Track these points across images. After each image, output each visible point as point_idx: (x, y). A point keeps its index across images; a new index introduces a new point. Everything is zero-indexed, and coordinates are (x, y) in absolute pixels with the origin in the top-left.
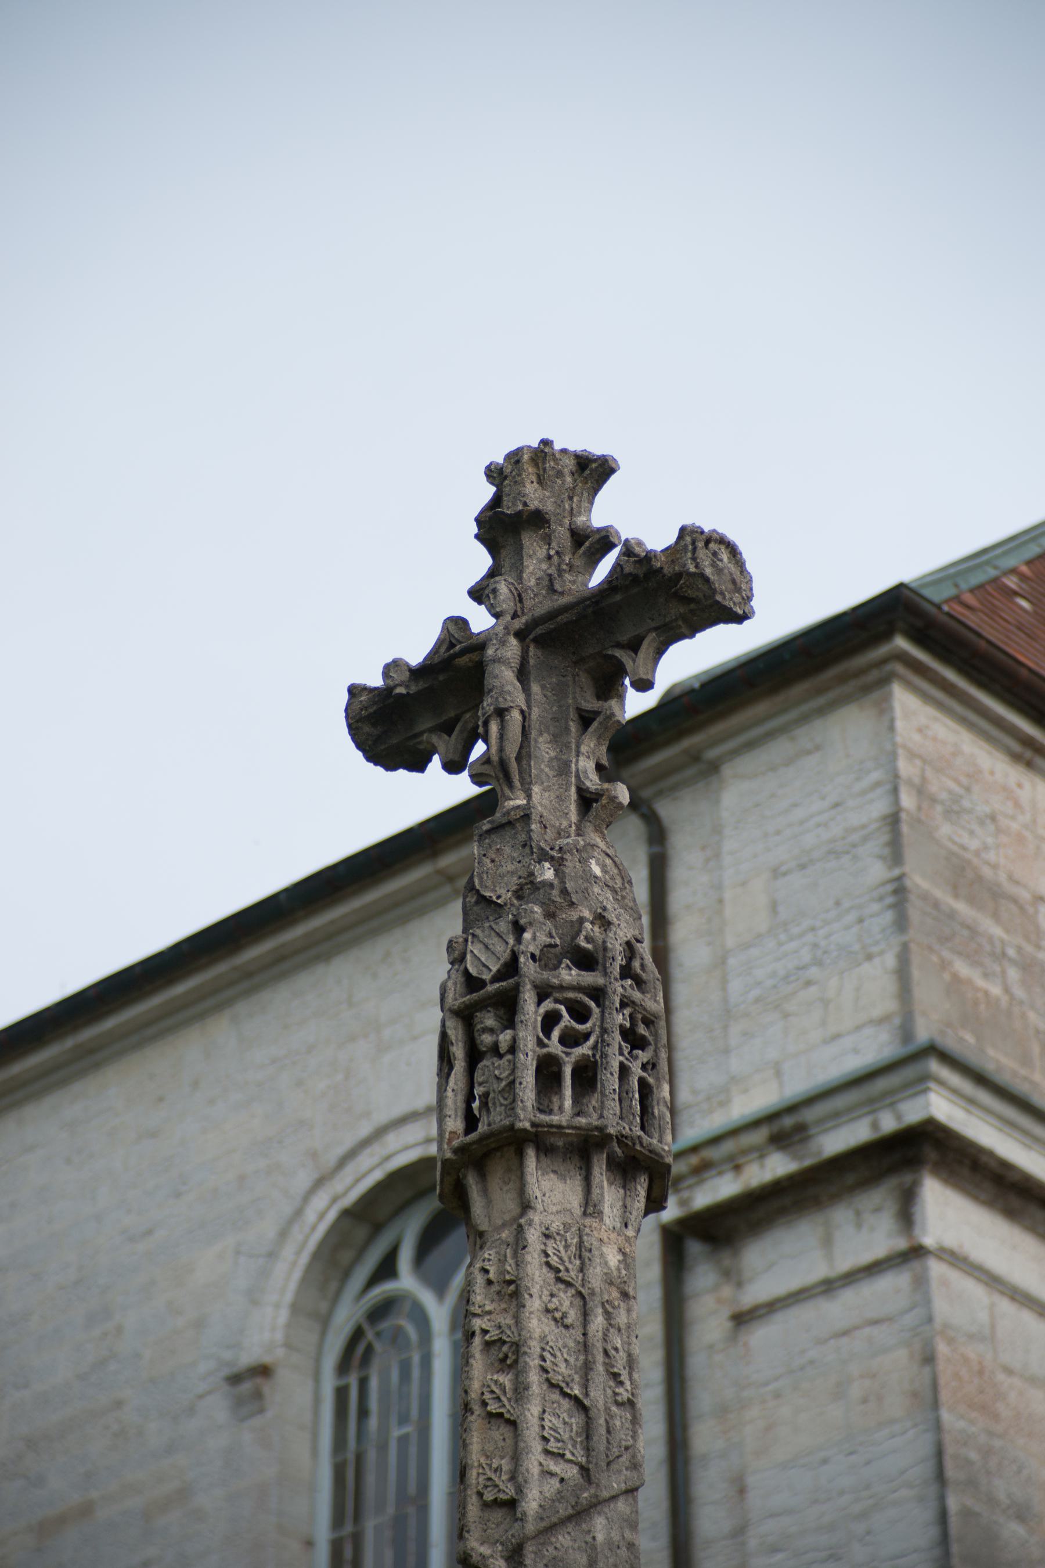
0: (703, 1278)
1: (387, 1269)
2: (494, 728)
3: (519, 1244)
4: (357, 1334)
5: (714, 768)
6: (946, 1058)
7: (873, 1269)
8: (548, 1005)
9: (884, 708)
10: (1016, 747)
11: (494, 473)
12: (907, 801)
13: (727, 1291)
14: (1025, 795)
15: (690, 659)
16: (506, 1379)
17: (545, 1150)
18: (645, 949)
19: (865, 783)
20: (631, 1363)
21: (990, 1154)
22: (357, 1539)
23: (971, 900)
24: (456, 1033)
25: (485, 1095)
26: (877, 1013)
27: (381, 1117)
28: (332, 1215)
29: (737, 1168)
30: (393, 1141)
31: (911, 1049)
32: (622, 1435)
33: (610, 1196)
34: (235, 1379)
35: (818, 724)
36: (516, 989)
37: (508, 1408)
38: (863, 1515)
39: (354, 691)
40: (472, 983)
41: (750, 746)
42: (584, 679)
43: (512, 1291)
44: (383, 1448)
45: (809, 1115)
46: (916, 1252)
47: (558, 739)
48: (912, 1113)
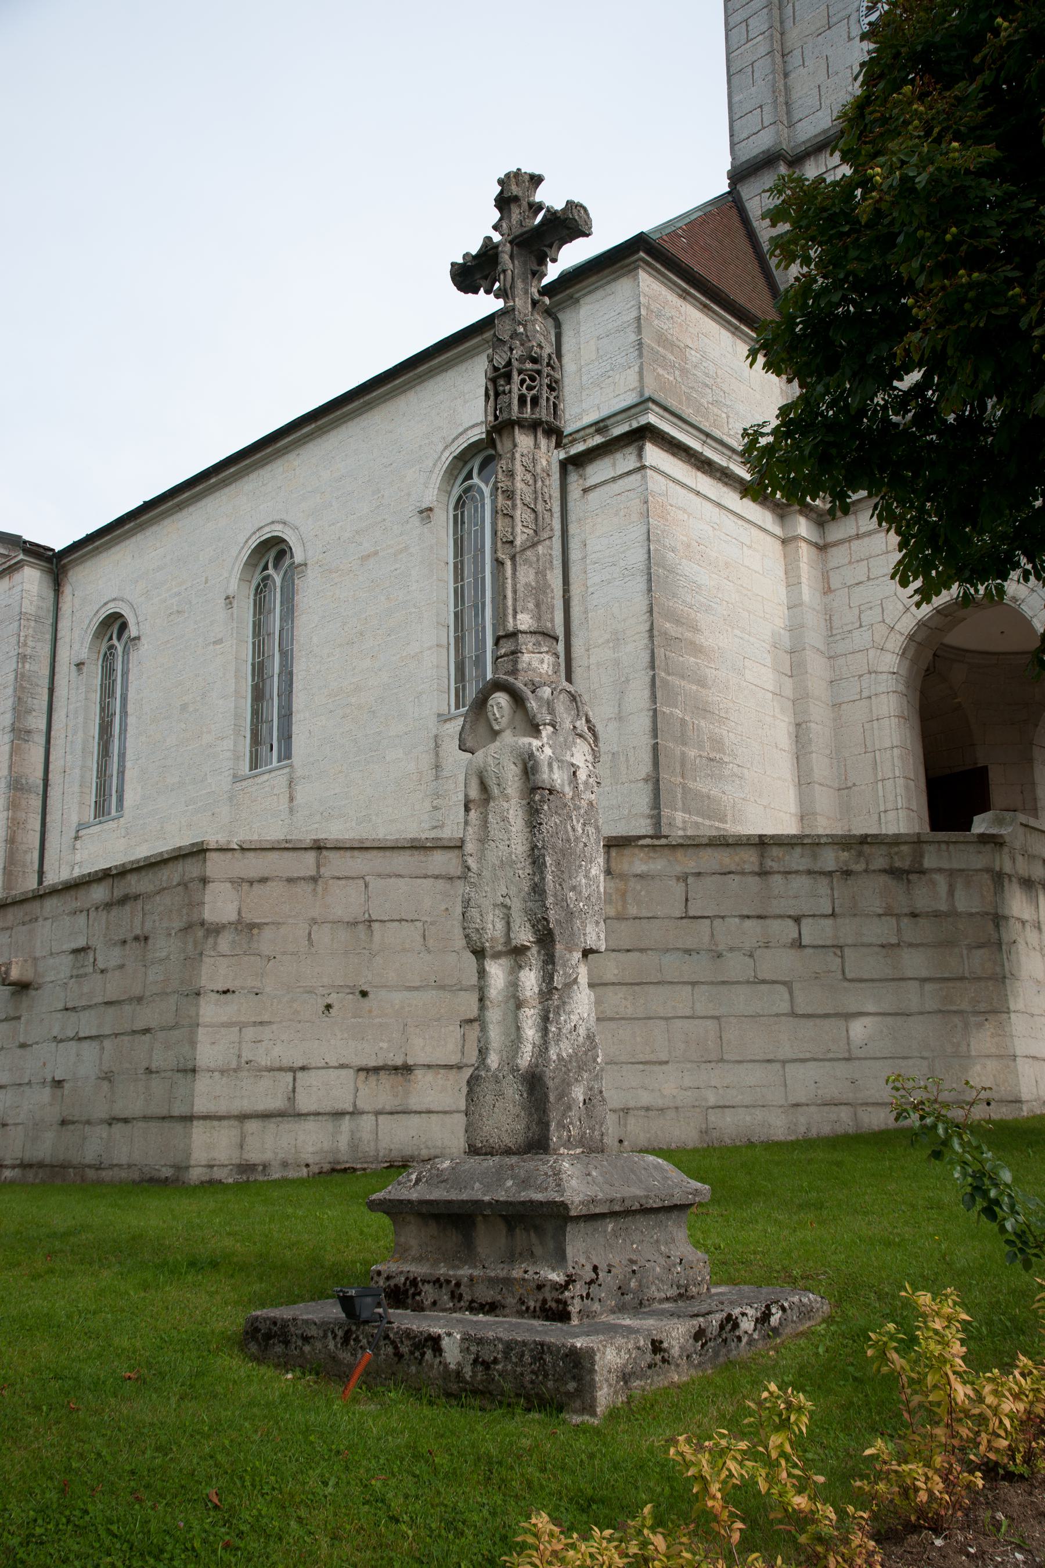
0: (573, 477)
1: (469, 476)
2: (502, 277)
3: (513, 458)
4: (460, 498)
5: (577, 301)
6: (654, 402)
7: (629, 473)
8: (522, 376)
9: (636, 278)
10: (681, 293)
11: (501, 182)
12: (643, 312)
13: (581, 481)
14: (683, 310)
15: (572, 255)
16: (509, 503)
17: (521, 426)
18: (554, 356)
19: (629, 306)
20: (550, 497)
21: (668, 434)
22: (462, 562)
23: (664, 347)
24: (490, 387)
25: (501, 409)
26: (631, 387)
27: (466, 425)
28: (450, 458)
29: (585, 441)
30: (470, 433)
31: (643, 399)
32: (548, 520)
33: (543, 442)
34: (421, 512)
35: (613, 284)
36: (511, 371)
37: (510, 512)
38: (624, 552)
39: (453, 264)
40: (496, 369)
41: (590, 292)
42: (533, 258)
43: (511, 474)
44: (469, 534)
45: (609, 422)
46: (643, 467)
47: (524, 281)
48: (643, 421)
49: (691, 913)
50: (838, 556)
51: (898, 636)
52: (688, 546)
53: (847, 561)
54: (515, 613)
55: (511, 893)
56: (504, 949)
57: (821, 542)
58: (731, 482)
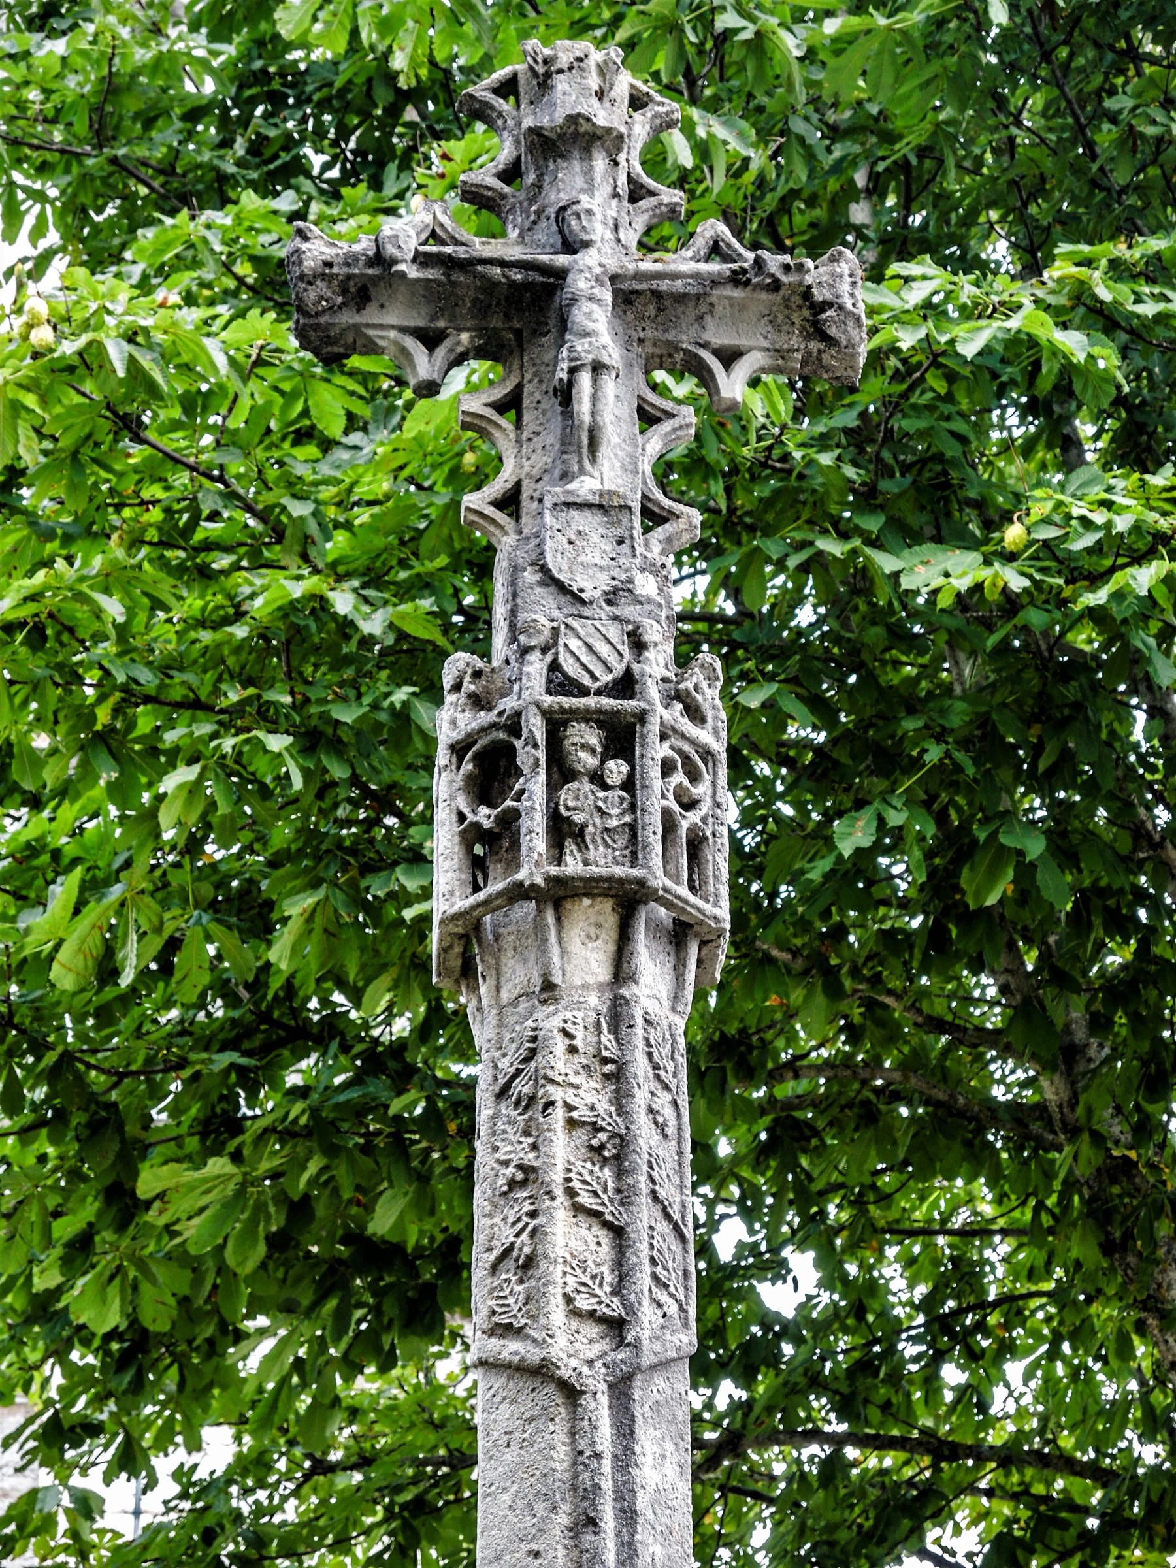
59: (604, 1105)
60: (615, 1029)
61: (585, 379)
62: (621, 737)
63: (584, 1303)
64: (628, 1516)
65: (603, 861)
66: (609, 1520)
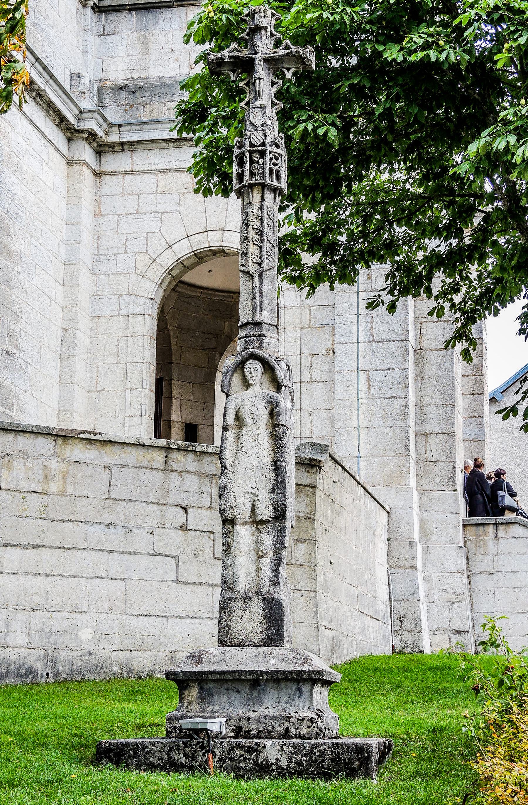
49: (112, 496)
50: (110, 184)
51: (159, 268)
52: (10, 157)
53: (119, 191)
54: (261, 308)
55: (259, 487)
56: (249, 520)
57: (97, 169)
58: (41, 103)
59: (259, 225)
60: (261, 210)
61: (257, 81)
62: (262, 154)
63: (254, 261)
64: (261, 297)
65: (258, 180)
66: (258, 298)
